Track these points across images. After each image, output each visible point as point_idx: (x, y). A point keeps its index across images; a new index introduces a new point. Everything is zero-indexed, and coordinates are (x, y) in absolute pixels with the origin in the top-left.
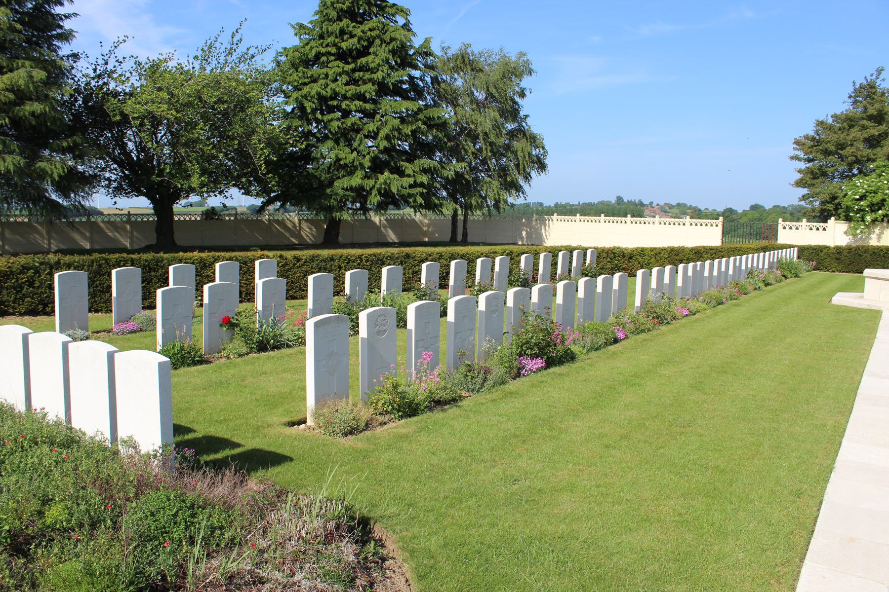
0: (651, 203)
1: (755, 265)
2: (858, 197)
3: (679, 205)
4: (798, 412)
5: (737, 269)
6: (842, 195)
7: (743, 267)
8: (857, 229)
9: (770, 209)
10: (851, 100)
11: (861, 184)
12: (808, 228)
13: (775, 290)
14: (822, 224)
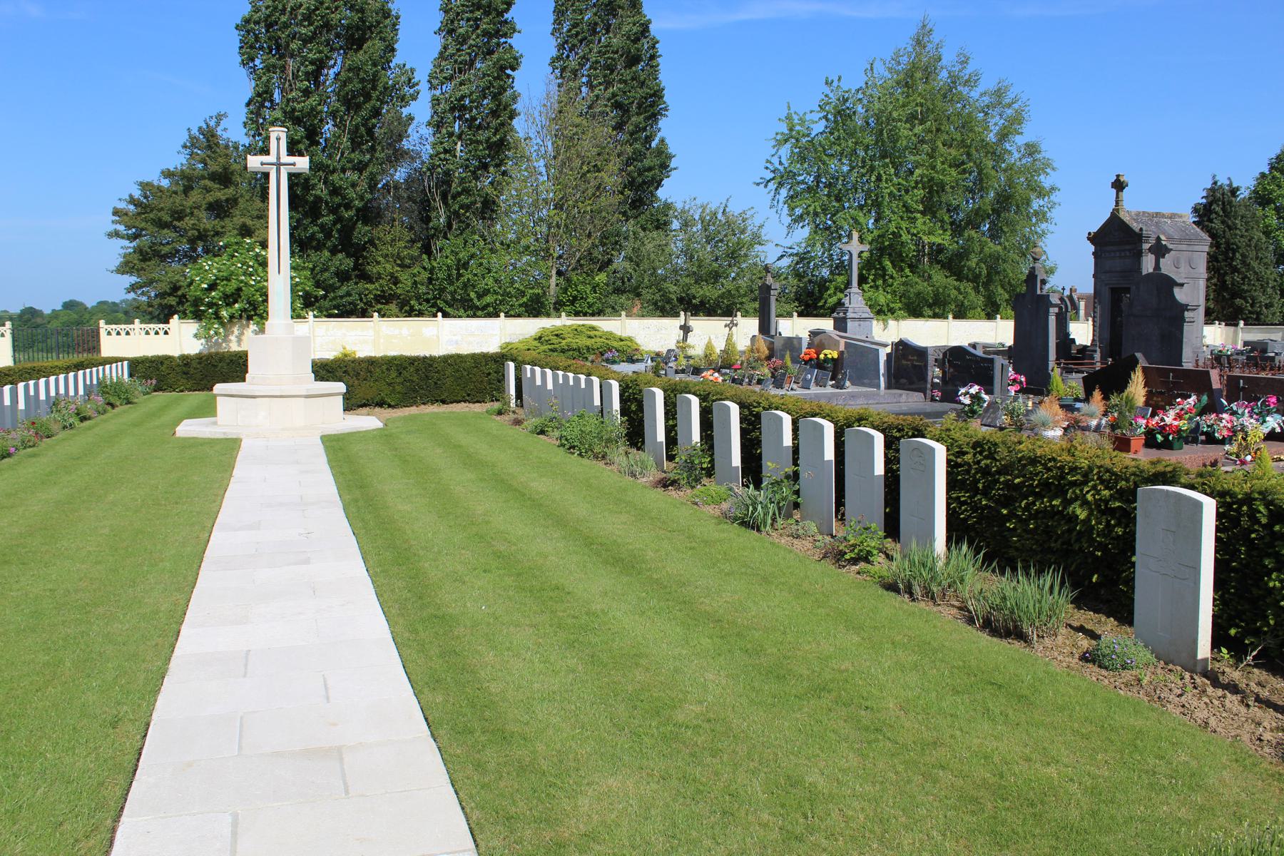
1: (62, 391)
2: (206, 286)
4: (119, 601)
5: (32, 401)
6: (185, 284)
7: (43, 397)
8: (209, 329)
9: (93, 307)
13: (96, 425)
14: (161, 326)
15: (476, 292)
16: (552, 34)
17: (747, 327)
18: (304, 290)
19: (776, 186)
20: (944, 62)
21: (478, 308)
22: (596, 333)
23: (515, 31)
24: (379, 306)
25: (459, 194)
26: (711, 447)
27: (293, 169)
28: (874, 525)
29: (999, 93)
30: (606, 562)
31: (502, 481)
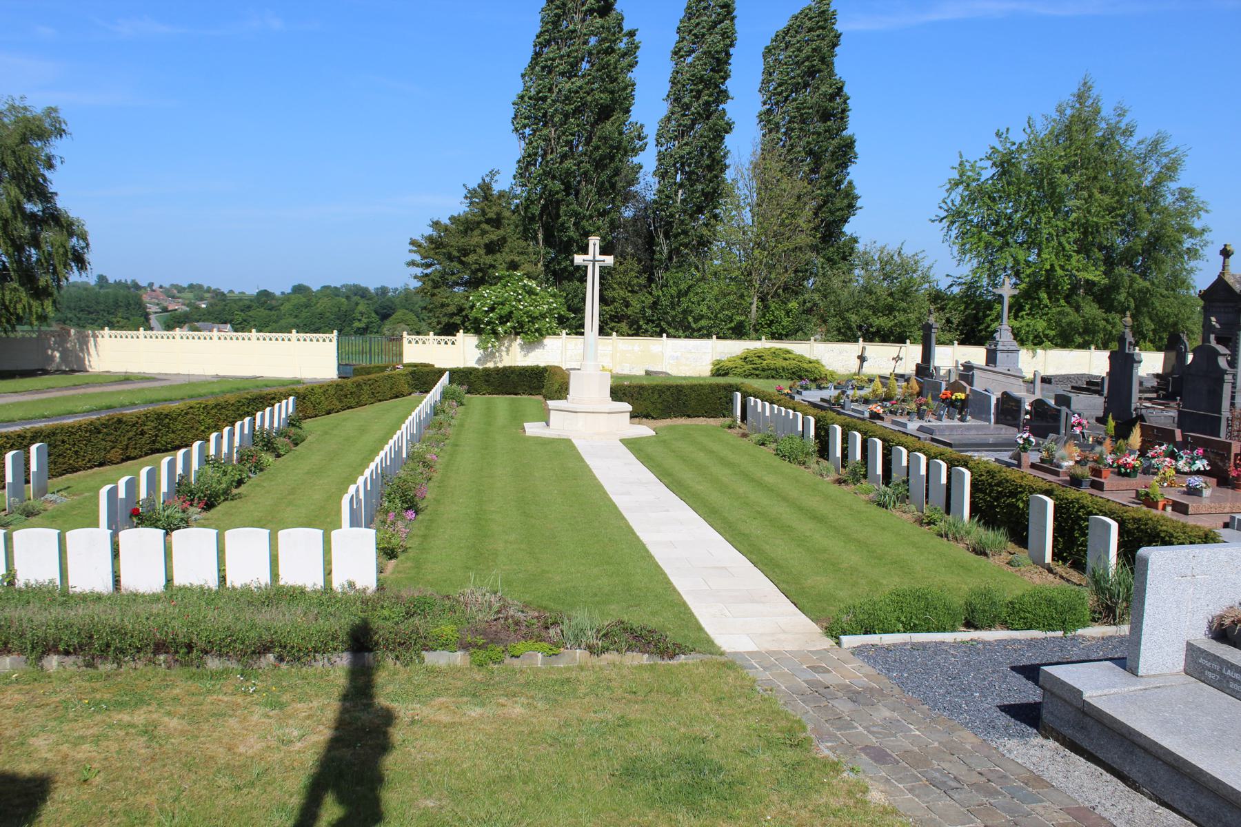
0: (151, 285)
2: (486, 309)
3: (191, 287)
8: (488, 342)
10: (468, 201)
11: (488, 294)
12: (436, 342)
15: (693, 317)
16: (760, 91)
17: (911, 354)
18: (559, 314)
19: (948, 223)
20: (1103, 114)
21: (694, 330)
22: (790, 356)
23: (728, 97)
24: (613, 324)
25: (679, 234)
26: (866, 463)
27: (602, 264)
28: (939, 508)
29: (1155, 145)
30: (810, 518)
31: (747, 475)
